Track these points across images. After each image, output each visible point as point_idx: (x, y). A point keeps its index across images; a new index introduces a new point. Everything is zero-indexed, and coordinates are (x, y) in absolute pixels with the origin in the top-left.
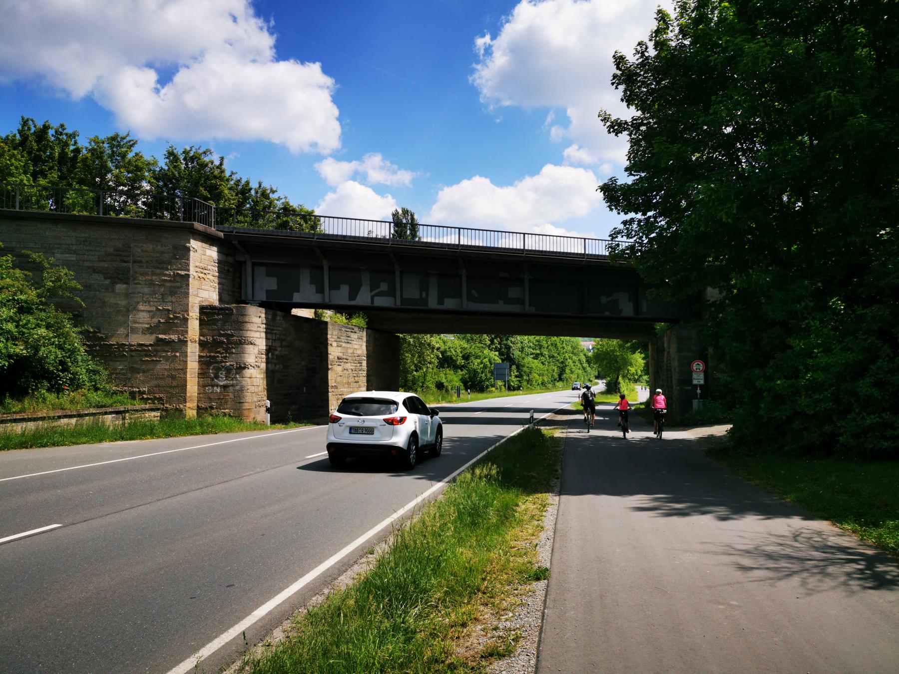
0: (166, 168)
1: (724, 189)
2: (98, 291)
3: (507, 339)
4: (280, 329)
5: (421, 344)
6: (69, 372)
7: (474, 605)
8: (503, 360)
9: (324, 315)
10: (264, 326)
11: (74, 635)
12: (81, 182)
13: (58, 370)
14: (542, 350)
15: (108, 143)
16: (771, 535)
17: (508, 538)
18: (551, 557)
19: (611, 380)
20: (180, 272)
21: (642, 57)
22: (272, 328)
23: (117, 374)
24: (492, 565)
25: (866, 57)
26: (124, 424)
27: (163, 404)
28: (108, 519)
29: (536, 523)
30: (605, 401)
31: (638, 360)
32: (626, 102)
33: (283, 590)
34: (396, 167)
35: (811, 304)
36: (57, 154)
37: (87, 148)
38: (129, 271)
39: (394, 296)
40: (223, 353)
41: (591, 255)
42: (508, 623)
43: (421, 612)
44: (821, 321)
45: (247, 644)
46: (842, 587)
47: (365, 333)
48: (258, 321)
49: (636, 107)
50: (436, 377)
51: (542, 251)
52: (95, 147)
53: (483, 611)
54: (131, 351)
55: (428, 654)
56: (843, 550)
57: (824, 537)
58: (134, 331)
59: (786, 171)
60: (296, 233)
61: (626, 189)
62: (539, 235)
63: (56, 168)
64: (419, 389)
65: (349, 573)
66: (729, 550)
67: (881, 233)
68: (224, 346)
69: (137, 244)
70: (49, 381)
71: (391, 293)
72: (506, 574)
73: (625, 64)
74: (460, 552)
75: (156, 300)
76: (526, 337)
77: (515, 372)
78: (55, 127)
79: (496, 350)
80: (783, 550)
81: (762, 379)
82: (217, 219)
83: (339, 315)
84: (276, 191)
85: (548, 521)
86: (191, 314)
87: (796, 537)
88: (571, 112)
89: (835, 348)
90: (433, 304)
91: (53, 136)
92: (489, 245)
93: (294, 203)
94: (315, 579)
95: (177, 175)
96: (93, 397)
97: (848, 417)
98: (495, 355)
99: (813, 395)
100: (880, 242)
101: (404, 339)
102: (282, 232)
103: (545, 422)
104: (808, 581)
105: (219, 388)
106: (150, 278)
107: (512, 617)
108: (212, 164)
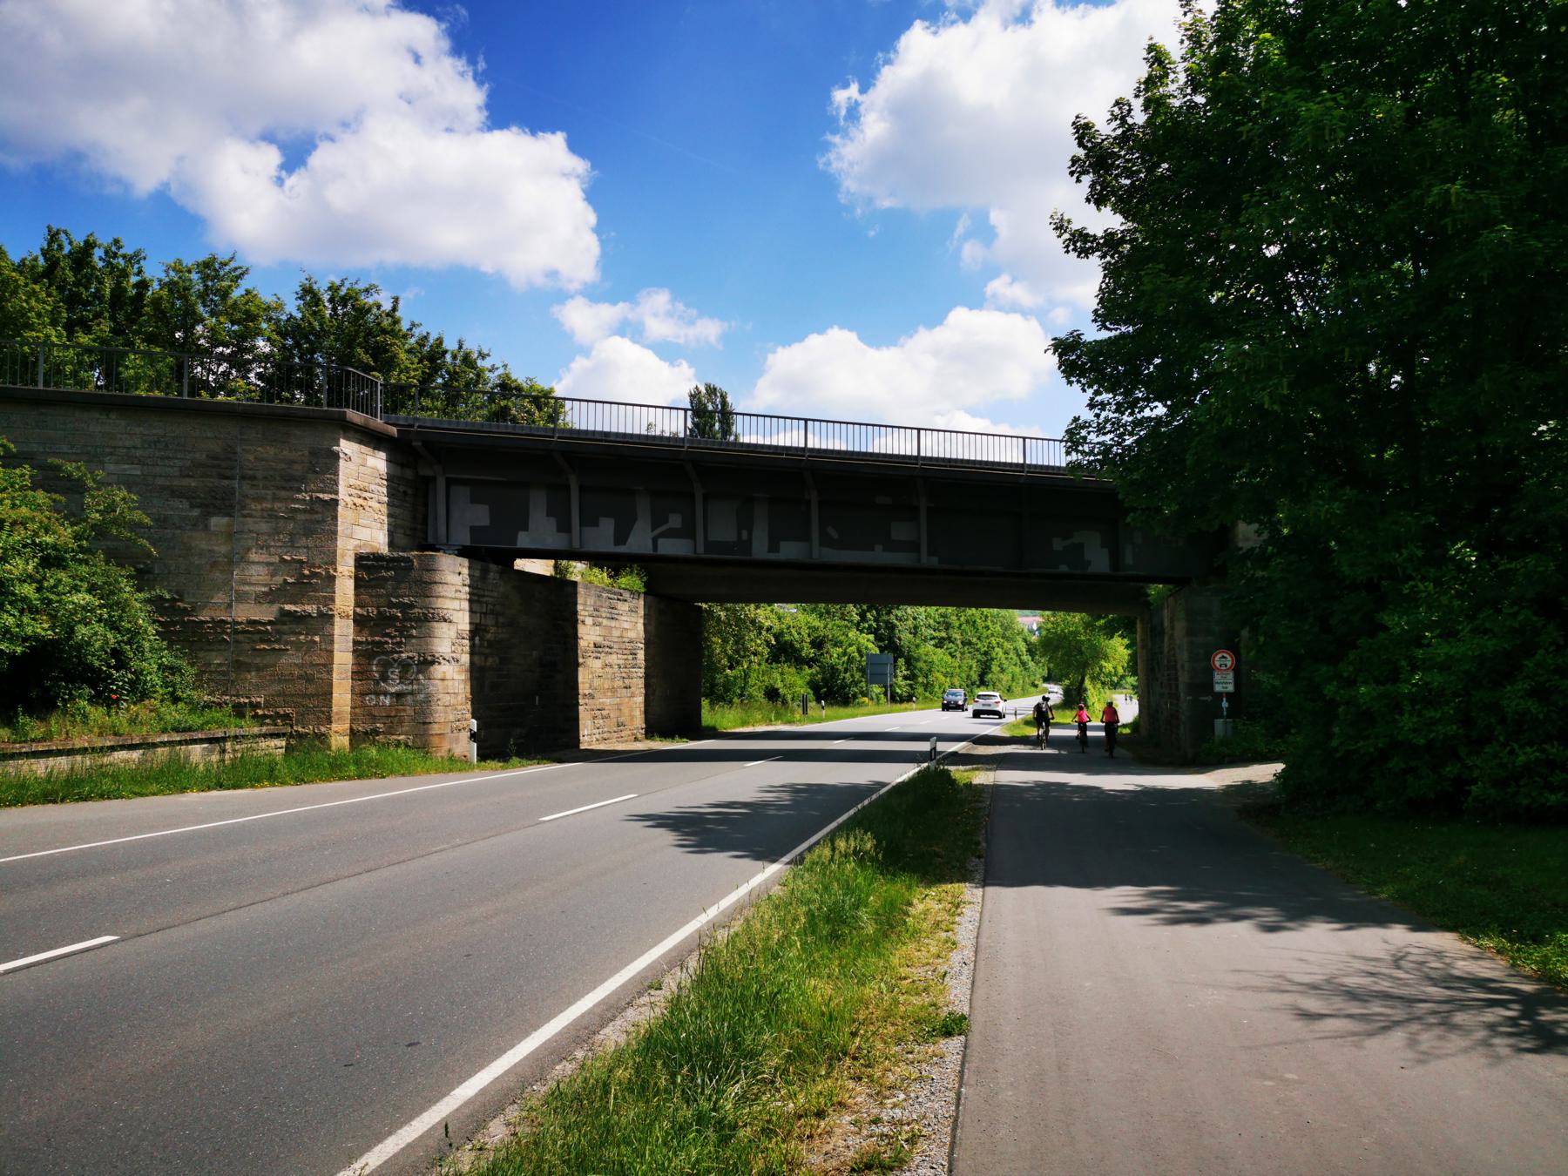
1: (1266, 353)
2: (180, 528)
3: (889, 613)
4: (496, 594)
6: (128, 669)
7: (837, 1079)
8: (882, 649)
9: (571, 570)
10: (467, 589)
11: (144, 1130)
13: (109, 666)
14: (951, 631)
16: (1355, 957)
18: (971, 995)
19: (1071, 684)
20: (321, 496)
22: (481, 592)
24: (867, 1008)
25: (1510, 127)
29: (943, 935)
31: (1118, 650)
33: (505, 1052)
36: (108, 291)
39: (693, 537)
40: (395, 637)
41: (1036, 466)
42: (897, 1111)
44: (1438, 583)
46: (1480, 1048)
47: (642, 602)
48: (457, 580)
50: (766, 678)
51: (950, 460)
53: (853, 1089)
54: (236, 632)
56: (1481, 983)
57: (1447, 960)
58: (242, 598)
62: (945, 431)
63: (107, 315)
64: (736, 700)
65: (618, 1022)
66: (1281, 985)
67: (1540, 429)
68: (398, 624)
71: (687, 532)
72: (893, 1024)
73: (1094, 137)
74: (812, 986)
75: (280, 544)
76: (922, 609)
77: (902, 671)
79: (870, 630)
80: (1376, 983)
81: (1335, 683)
83: (596, 570)
84: (488, 355)
85: (965, 932)
86: (340, 569)
87: (1397, 961)
89: (1462, 630)
92: (857, 449)
93: (519, 376)
94: (560, 1033)
95: (318, 328)
96: (170, 714)
97: (1486, 750)
98: (868, 640)
99: (1424, 712)
100: (1538, 444)
101: (710, 613)
103: (956, 758)
106: (269, 506)
107: (905, 1100)
108: (379, 309)
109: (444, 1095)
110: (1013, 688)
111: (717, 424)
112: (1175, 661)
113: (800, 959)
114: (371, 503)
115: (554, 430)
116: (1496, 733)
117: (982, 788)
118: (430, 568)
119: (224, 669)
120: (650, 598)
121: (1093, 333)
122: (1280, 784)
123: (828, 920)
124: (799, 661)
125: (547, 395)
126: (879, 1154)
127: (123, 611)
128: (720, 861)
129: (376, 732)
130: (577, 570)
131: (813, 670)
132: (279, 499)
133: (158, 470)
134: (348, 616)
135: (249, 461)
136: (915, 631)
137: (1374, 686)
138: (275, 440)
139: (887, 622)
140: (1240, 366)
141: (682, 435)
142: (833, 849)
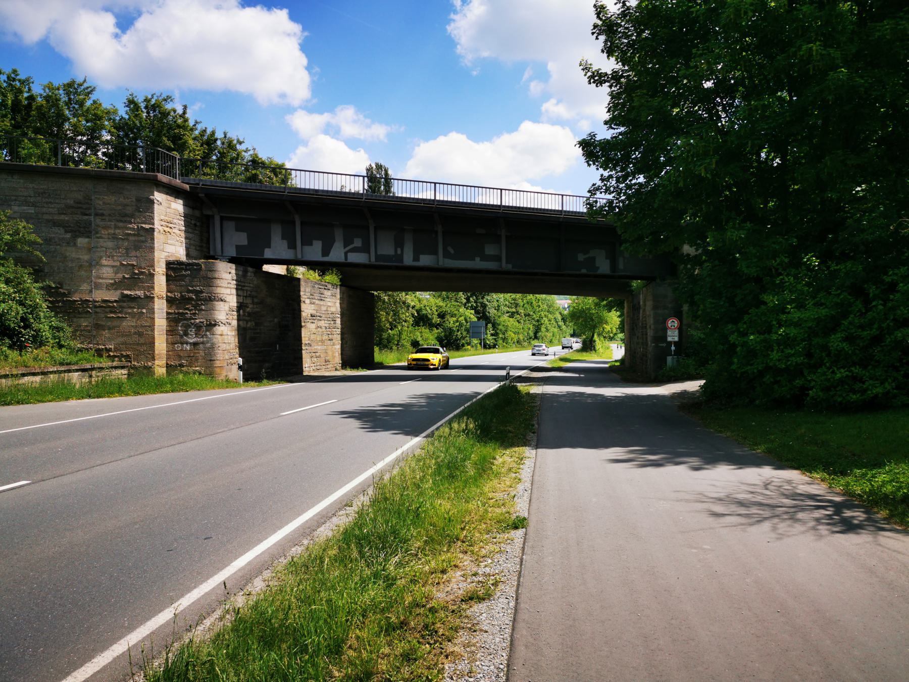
0: (127, 117)
1: (704, 144)
2: (59, 245)
3: (483, 298)
4: (251, 285)
5: (396, 302)
6: (32, 329)
7: (453, 553)
8: (479, 319)
9: (296, 271)
10: (235, 282)
11: (49, 588)
12: (37, 131)
13: (19, 327)
14: (518, 308)
15: (64, 90)
16: (742, 483)
17: (486, 489)
18: (529, 507)
19: (587, 338)
20: (144, 226)
21: (623, 7)
22: (243, 284)
23: (81, 331)
24: (470, 515)
25: (848, 11)
26: (90, 382)
27: (131, 362)
28: (79, 475)
29: (514, 475)
30: (580, 358)
31: (614, 318)
32: (607, 53)
33: (262, 541)
34: (368, 121)
35: (786, 260)
36: (10, 102)
37: (41, 95)
38: (90, 224)
39: (369, 252)
40: (192, 310)
41: (569, 212)
42: (487, 568)
43: (400, 561)
44: (796, 277)
45: (228, 593)
46: (811, 531)
47: (338, 290)
48: (229, 277)
49: (616, 60)
50: (411, 335)
51: (519, 208)
52: (50, 94)
53: (462, 558)
54: (95, 307)
55: (408, 599)
56: (812, 497)
57: (794, 485)
58: (98, 286)
59: (766, 127)
60: (266, 186)
61: (606, 145)
62: (516, 191)
63: (9, 116)
64: (394, 347)
65: (327, 524)
66: (702, 498)
67: (857, 189)
68: (193, 303)
69: (98, 196)
70: (11, 338)
71: (365, 249)
72: (485, 523)
73: (606, 14)
74: (439, 503)
75: (120, 254)
76: (501, 295)
77: (490, 330)
78: (7, 72)
79: (472, 308)
80: (754, 497)
81: (736, 334)
82: (182, 170)
83: (311, 272)
84: (243, 142)
85: (526, 472)
86: (157, 269)
87: (766, 486)
88: (551, 66)
89: (808, 304)
90: (408, 259)
91: (4, 82)
92: (465, 201)
93: (263, 156)
94: (294, 531)
95: (138, 125)
96: (58, 355)
97: (819, 371)
98: (471, 313)
99: (784, 350)
100: (856, 199)
101: (379, 297)
102: (251, 185)
103: (521, 379)
104: (778, 526)
105: (189, 345)
106: (113, 232)
107: (492, 563)
108: (175, 113)
109: (226, 566)
110: (553, 340)
111: (382, 187)
112: (646, 324)
113: (432, 489)
114: (174, 230)
115: (285, 188)
116: (825, 361)
117: (535, 396)
118: (212, 270)
119: (89, 328)
120: (344, 288)
121: (605, 134)
122: (703, 391)
123: (449, 468)
124: (431, 325)
125: (281, 167)
126: (477, 591)
127: (27, 294)
128: (385, 437)
129: (181, 365)
130: (300, 271)
131: (439, 331)
132: (119, 228)
133: (44, 210)
134: (163, 298)
135: (100, 204)
136: (498, 308)
137: (757, 335)
138: (114, 193)
139: (482, 303)
140: (689, 152)
141: (361, 192)
142: (451, 429)
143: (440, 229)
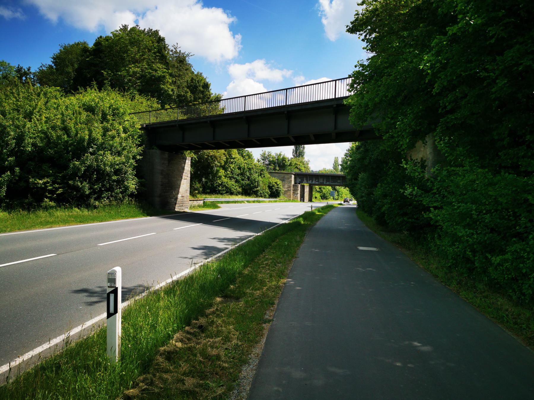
71: (318, 181)
143: (330, 178)
